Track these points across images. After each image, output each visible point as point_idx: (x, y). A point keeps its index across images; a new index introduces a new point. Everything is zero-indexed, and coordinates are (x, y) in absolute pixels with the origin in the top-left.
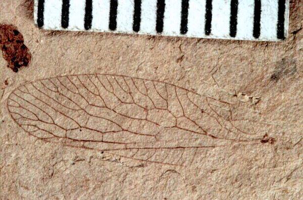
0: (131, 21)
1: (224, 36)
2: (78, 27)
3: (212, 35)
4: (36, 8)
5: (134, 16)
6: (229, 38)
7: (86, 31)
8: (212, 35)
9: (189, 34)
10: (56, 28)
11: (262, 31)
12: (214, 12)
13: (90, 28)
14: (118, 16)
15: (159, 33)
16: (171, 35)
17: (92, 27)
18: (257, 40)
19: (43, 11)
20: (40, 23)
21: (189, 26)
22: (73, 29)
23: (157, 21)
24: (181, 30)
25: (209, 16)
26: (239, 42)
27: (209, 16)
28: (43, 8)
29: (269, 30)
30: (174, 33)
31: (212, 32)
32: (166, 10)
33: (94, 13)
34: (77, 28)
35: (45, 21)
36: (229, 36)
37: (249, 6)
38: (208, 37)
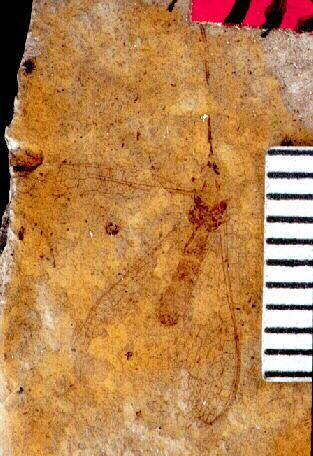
0: (276, 171)
12: (288, 311)
20: (272, 153)
21: (274, 290)
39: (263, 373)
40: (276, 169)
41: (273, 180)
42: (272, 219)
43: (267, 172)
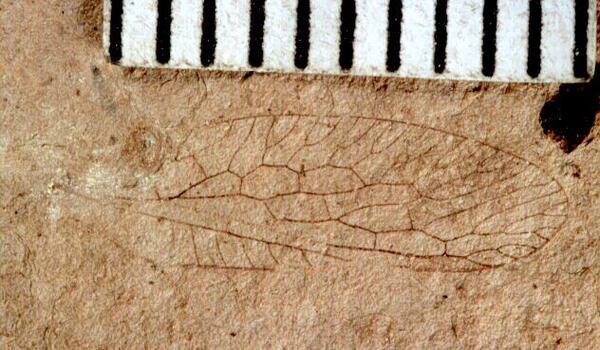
4: (107, 25)
9: (403, 72)
11: (544, 64)
20: (116, 54)
31: (448, 66)
32: (198, 42)
39: (578, 80)
40: (291, 47)
41: (451, 63)
42: (393, 61)
43: (528, 79)
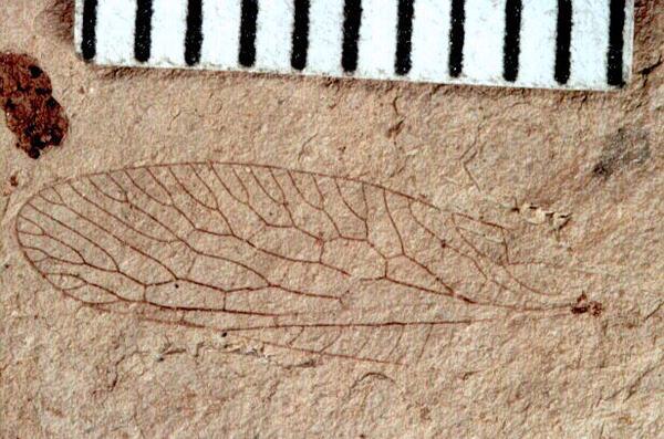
0: (288, 46)
1: (492, 80)
2: (171, 60)
3: (465, 76)
4: (79, 18)
5: (295, 35)
6: (502, 83)
7: (187, 68)
8: (465, 76)
9: (414, 75)
10: (123, 60)
12: (468, 26)
13: (198, 60)
14: (259, 34)
15: (349, 73)
16: (376, 76)
17: (202, 60)
18: (563, 87)
19: (94, 24)
22: (159, 63)
23: (345, 46)
24: (396, 65)
25: (457, 36)
26: (524, 91)
27: (457, 36)
28: (94, 18)
29: (589, 67)
30: (381, 71)
33: (206, 28)
34: (169, 62)
35: (99, 47)
36: (502, 79)
37: (546, 13)
38: (456, 81)
